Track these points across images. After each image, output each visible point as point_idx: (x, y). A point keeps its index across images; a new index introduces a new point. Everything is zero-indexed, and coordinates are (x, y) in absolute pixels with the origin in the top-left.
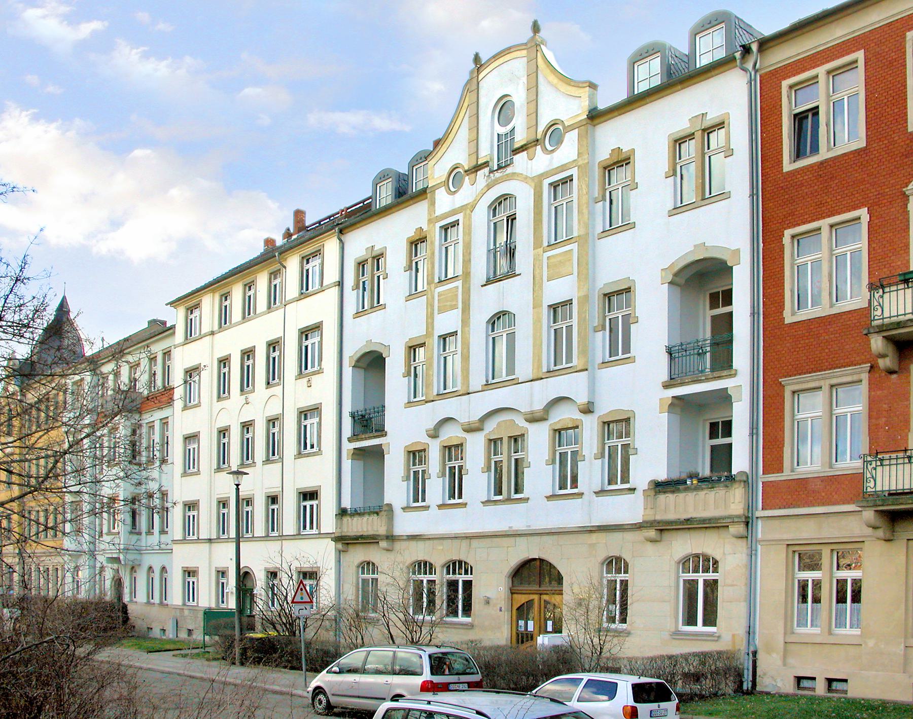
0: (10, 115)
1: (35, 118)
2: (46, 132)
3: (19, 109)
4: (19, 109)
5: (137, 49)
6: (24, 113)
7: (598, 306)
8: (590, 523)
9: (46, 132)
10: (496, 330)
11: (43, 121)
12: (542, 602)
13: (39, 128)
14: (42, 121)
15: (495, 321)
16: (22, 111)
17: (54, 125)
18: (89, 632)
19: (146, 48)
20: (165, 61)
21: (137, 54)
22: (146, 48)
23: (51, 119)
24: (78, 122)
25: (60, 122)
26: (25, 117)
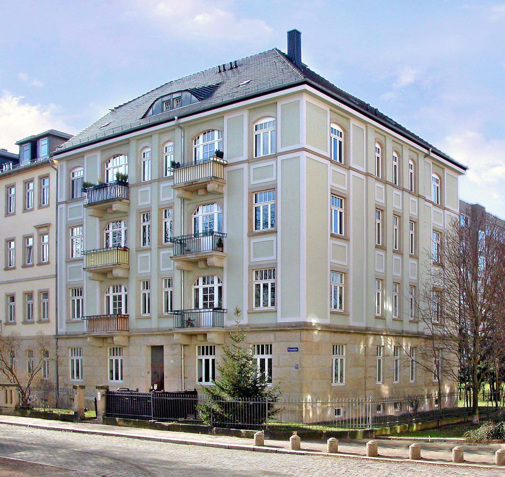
0: (5, 99)
1: (22, 102)
2: (29, 112)
3: (11, 96)
4: (11, 96)
5: (17, 97)
6: (15, 99)
7: (203, 256)
8: (278, 366)
9: (29, 112)
10: (196, 144)
11: (28, 104)
12: (266, 269)
13: (25, 109)
14: (27, 104)
15: (196, 139)
16: (14, 97)
17: (35, 108)
18: (237, 366)
19: (23, 97)
20: (36, 106)
21: (17, 100)
22: (23, 97)
23: (33, 104)
24: (52, 106)
25: (40, 105)
26: (15, 101)
